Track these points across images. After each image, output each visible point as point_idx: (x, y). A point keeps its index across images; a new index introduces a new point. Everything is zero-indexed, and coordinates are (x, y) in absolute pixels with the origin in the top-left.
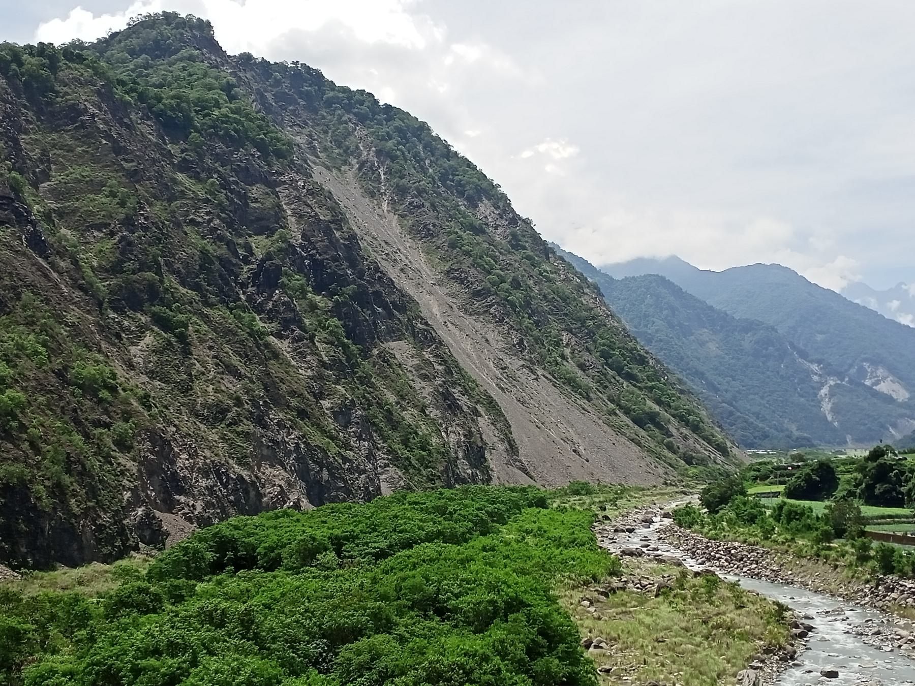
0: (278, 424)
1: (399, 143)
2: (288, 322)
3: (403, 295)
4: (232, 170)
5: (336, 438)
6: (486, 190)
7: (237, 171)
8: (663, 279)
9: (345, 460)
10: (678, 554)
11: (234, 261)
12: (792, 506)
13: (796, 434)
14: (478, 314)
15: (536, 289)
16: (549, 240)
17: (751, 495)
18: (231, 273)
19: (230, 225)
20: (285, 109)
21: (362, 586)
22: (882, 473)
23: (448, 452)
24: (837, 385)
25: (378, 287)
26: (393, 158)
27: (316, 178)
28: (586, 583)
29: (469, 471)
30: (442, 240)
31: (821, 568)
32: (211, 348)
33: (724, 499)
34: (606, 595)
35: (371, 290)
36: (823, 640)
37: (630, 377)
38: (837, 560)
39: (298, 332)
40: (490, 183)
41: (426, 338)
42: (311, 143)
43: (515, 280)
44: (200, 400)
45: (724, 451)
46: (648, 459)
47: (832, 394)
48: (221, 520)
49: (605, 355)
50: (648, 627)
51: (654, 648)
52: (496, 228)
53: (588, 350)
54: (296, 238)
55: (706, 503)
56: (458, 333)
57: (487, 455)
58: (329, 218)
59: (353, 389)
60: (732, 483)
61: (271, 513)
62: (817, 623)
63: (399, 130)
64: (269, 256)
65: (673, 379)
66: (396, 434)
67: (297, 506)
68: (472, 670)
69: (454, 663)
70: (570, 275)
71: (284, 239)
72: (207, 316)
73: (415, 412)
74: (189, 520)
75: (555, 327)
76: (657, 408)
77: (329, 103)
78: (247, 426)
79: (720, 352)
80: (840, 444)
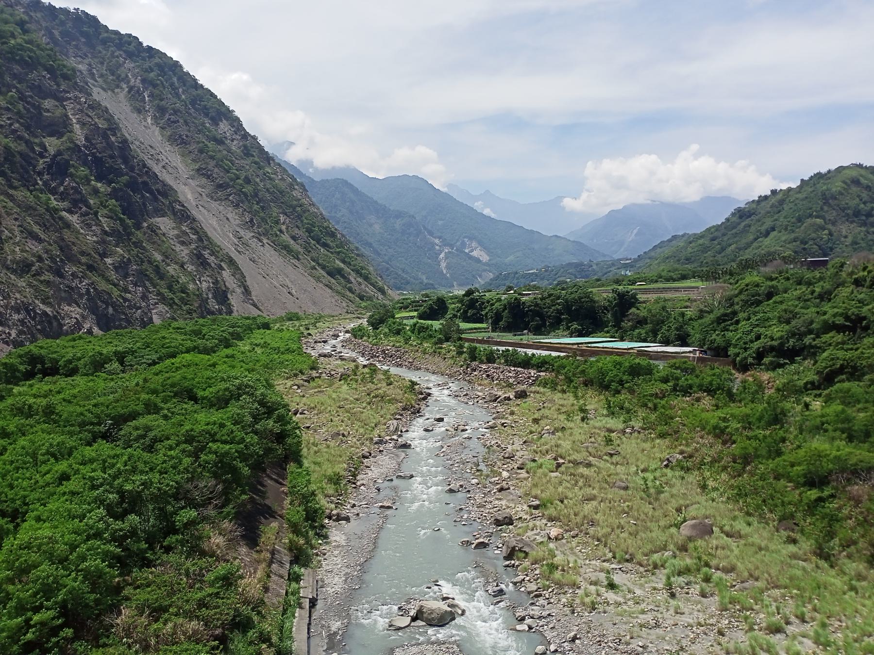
0: (72, 275)
1: (159, 75)
2: (77, 203)
3: (164, 184)
4: (28, 87)
5: (118, 285)
6: (222, 113)
7: (32, 87)
8: (346, 182)
9: (125, 300)
10: (354, 355)
11: (32, 155)
13: (425, 281)
14: (221, 200)
15: (262, 185)
16: (270, 152)
18: (30, 164)
19: (28, 128)
20: (70, 44)
21: (137, 384)
23: (201, 294)
24: (450, 252)
25: (145, 178)
26: (155, 86)
27: (95, 96)
28: (296, 375)
29: (217, 307)
30: (193, 147)
31: (437, 359)
32: (16, 219)
33: (382, 321)
34: (308, 382)
35: (140, 180)
36: (436, 400)
37: (325, 245)
39: (84, 209)
40: (227, 108)
41: (183, 216)
42: (90, 70)
43: (246, 177)
44: (9, 258)
45: (383, 291)
46: (337, 297)
47: (446, 258)
48: (32, 342)
49: (309, 231)
50: (334, 399)
51: (337, 412)
52: (232, 141)
53: (297, 227)
54: (81, 139)
55: (371, 323)
56: (206, 213)
57: (229, 296)
58: (105, 126)
59: (129, 251)
60: (387, 311)
61: (70, 337)
62: (435, 391)
63: (158, 65)
64: (59, 153)
65: (352, 247)
66: (163, 282)
67: (90, 332)
68: (215, 434)
69: (203, 430)
70: (285, 176)
71: (72, 142)
72: (12, 196)
73: (177, 267)
74: (7, 343)
75: (275, 211)
76: (342, 265)
77: (104, 42)
78: (47, 276)
79: (381, 231)
80: (450, 287)
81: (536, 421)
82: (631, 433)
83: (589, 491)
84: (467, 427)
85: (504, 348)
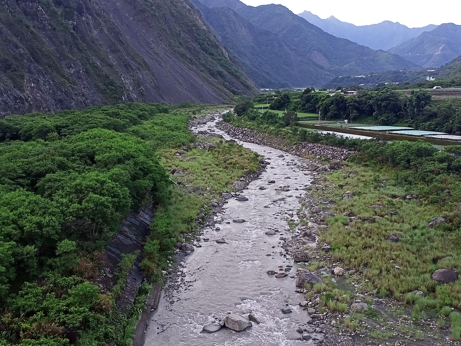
10: (221, 133)
12: (270, 113)
17: (255, 108)
22: (308, 100)
28: (179, 146)
34: (187, 151)
38: (284, 136)
55: (236, 111)
81: (341, 186)
82: (410, 199)
83: (368, 240)
84: (290, 188)
85: (325, 132)
